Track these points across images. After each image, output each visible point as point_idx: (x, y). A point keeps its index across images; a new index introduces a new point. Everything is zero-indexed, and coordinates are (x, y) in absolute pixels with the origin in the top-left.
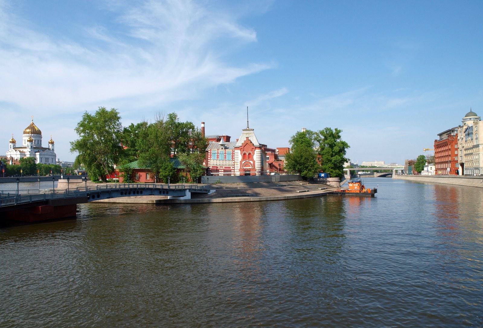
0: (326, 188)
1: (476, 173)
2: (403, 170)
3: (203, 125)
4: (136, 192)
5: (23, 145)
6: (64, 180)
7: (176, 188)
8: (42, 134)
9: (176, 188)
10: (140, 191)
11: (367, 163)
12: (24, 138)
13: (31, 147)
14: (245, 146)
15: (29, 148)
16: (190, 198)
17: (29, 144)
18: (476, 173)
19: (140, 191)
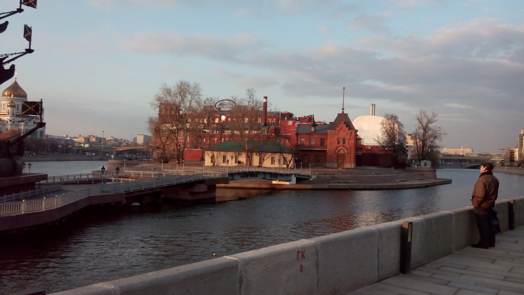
0: (405, 180)
1: (221, 170)
2: (502, 161)
3: (264, 100)
4: (249, 175)
5: (2, 111)
6: (114, 160)
7: (75, 179)
8: (27, 98)
9: (75, 179)
10: (255, 174)
11: (449, 149)
12: (3, 102)
13: (13, 114)
14: (339, 130)
15: (9, 115)
16: (295, 183)
17: (10, 110)
18: (221, 170)
19: (255, 174)
